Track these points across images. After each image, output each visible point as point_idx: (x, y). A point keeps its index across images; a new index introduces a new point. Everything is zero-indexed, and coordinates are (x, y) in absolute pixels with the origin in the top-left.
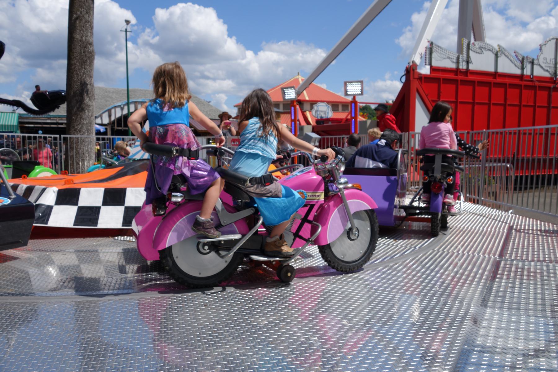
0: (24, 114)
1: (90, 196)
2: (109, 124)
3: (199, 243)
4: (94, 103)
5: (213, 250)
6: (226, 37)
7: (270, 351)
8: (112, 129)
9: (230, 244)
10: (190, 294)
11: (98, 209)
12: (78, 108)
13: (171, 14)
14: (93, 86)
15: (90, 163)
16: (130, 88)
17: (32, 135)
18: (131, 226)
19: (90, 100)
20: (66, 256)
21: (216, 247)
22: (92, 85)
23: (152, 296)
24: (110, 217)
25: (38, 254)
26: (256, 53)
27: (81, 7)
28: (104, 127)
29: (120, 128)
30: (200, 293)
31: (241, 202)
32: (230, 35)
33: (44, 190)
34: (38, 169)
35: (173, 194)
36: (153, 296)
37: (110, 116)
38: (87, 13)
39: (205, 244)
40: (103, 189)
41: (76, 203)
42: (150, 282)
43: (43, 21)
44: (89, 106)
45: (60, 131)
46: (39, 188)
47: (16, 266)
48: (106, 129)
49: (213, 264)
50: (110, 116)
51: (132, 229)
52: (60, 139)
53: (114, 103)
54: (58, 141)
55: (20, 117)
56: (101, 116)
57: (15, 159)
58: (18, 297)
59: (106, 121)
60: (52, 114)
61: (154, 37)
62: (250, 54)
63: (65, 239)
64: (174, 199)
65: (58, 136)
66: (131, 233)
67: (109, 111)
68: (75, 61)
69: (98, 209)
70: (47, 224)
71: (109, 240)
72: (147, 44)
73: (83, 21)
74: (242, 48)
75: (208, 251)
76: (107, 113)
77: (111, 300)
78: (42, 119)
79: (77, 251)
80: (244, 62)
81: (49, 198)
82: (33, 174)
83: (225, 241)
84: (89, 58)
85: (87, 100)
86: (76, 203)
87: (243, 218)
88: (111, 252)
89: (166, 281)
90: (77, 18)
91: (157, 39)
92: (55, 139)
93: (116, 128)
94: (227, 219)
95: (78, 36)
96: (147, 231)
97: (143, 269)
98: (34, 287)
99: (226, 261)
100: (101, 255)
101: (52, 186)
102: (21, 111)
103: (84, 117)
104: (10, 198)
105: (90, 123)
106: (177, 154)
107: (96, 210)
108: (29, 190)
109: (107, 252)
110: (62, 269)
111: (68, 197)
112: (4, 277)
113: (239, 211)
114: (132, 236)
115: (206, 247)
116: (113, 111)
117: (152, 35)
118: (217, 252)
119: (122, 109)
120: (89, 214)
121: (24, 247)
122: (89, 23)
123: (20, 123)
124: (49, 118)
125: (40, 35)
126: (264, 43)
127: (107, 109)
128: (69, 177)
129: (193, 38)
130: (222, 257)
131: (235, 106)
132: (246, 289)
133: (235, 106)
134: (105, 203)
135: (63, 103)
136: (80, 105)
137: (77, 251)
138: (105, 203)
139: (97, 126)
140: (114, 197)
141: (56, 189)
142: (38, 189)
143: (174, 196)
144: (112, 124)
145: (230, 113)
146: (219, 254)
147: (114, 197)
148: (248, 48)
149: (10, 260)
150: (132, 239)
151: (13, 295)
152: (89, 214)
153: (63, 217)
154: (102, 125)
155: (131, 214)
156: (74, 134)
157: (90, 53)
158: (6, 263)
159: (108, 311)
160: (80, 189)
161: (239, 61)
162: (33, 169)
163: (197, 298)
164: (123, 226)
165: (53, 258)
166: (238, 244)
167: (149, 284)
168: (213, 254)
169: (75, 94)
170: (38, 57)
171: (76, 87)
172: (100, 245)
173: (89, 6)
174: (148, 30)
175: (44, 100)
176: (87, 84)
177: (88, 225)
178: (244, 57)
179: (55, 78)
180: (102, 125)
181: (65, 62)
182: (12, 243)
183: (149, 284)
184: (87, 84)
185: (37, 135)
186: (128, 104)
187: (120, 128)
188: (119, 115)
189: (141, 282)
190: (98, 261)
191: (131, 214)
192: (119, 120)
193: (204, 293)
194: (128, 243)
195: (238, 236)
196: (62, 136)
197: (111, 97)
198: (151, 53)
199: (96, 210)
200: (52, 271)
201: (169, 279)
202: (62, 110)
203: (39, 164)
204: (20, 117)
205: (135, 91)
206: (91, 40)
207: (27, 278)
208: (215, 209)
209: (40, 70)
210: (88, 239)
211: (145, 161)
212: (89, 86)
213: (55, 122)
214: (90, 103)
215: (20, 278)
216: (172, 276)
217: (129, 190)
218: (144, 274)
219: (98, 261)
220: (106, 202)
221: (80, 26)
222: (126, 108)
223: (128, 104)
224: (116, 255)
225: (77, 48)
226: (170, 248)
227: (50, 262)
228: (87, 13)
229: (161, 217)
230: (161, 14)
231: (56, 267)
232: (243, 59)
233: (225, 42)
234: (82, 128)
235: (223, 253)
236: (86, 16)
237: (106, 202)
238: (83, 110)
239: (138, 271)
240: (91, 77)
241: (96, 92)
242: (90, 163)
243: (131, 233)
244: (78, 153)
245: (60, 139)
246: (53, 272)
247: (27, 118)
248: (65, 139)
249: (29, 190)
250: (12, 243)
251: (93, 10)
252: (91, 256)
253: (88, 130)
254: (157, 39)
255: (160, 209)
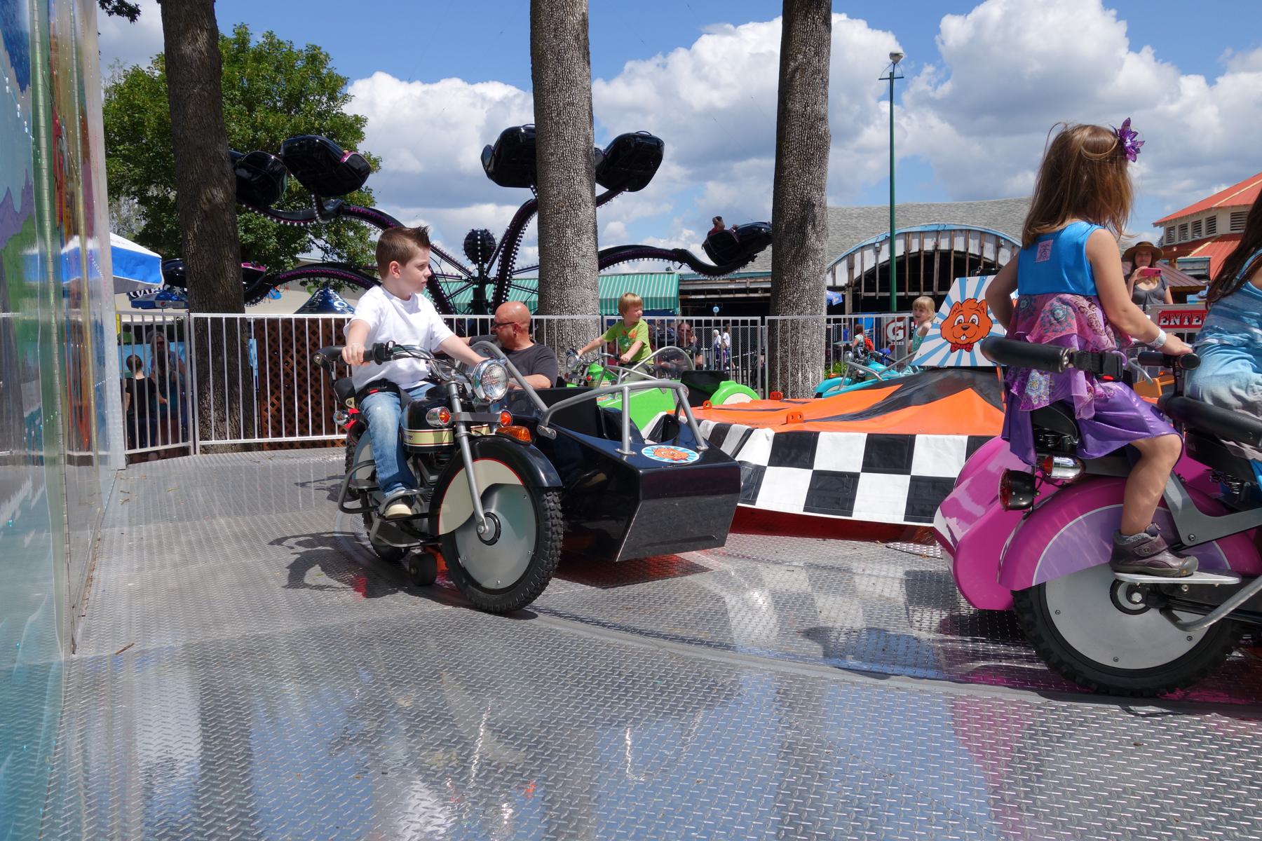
0: (689, 275)
1: (840, 450)
2: (848, 285)
3: (1116, 584)
4: (826, 245)
5: (1155, 606)
6: (1123, 51)
7: (1094, 816)
8: (856, 298)
9: (1204, 599)
10: (1089, 706)
11: (854, 477)
12: (794, 257)
13: (979, 25)
14: (825, 208)
15: (815, 375)
16: (896, 204)
17: (703, 318)
18: (931, 521)
19: (818, 239)
20: (795, 575)
21: (1164, 599)
22: (822, 206)
23: (971, 692)
24: (881, 499)
25: (741, 564)
26: (1211, 82)
27: (806, 43)
28: (839, 294)
29: (873, 294)
30: (1116, 708)
31: (1241, 487)
32: (1135, 47)
33: (748, 434)
34: (726, 387)
35: (1056, 460)
36: (999, 695)
37: (851, 269)
38: (816, 54)
39: (1132, 588)
40: (865, 436)
41: (809, 465)
42: (984, 659)
43: (715, 86)
44: (816, 251)
45: (762, 306)
46: (738, 429)
47: (706, 585)
48: (843, 296)
49: (1154, 641)
50: (851, 269)
51: (933, 528)
52: (763, 323)
53: (860, 240)
54: (759, 326)
55: (682, 280)
56: (832, 270)
57: (685, 368)
58: (719, 652)
59: (842, 280)
60: (742, 270)
61: (941, 82)
62: (1192, 85)
63: (788, 538)
64: (1057, 473)
65: (758, 318)
66: (932, 536)
67: (850, 257)
68: (789, 160)
69: (854, 477)
70: (753, 503)
71: (876, 548)
72: (924, 102)
73: (809, 73)
74: (1168, 70)
75: (1142, 606)
76: (845, 263)
77: (903, 689)
78: (720, 283)
79: (810, 566)
80: (1174, 108)
81: (757, 451)
82: (716, 399)
83: (1191, 586)
84: (819, 148)
85: (812, 240)
86: (809, 465)
87: (1244, 533)
88: (881, 575)
89: (1022, 663)
90: (796, 70)
91: (947, 88)
92: (754, 323)
93: (863, 294)
94: (1201, 527)
95: (797, 107)
96: (984, 537)
97: (954, 625)
98: (735, 635)
99: (1190, 638)
100: (857, 579)
101: (764, 426)
102: (686, 269)
103: (805, 275)
104: (697, 451)
105: (818, 288)
106: (1071, 366)
107: (849, 481)
108: (720, 433)
109: (877, 577)
110: (781, 602)
111: (796, 449)
112: (688, 605)
113: (1232, 510)
114: (933, 544)
115: (1137, 597)
116: (858, 256)
117: (935, 80)
118: (1166, 611)
119: (877, 251)
120: (835, 489)
121: (720, 549)
122: (821, 74)
123: (681, 292)
124: (732, 281)
125: (711, 113)
126: (1229, 52)
127: (845, 253)
128: (789, 407)
129: (1036, 67)
130: (1184, 627)
131: (1155, 225)
132: (1249, 720)
133: (1155, 225)
134: (869, 466)
135: (763, 248)
136: (798, 252)
137: (810, 566)
138: (869, 466)
139: (828, 293)
140: (889, 454)
141: (770, 433)
142: (736, 432)
143: (1058, 465)
144: (855, 285)
145: (624, 199)
146: (1174, 620)
147: (889, 454)
148: (1186, 70)
149: (694, 572)
150: (936, 550)
151: (709, 644)
152: (835, 489)
153: (784, 491)
154: (833, 289)
155: (928, 495)
156: (777, 314)
157: (821, 138)
158: (689, 577)
159: (901, 713)
160: (817, 434)
161: (1160, 107)
162: (717, 387)
163: (1108, 717)
164: (906, 520)
165: (764, 573)
166: (1230, 601)
167: (983, 663)
168: (1153, 615)
169: (792, 227)
170: (715, 157)
171: (793, 211)
172: (859, 558)
173: (821, 38)
174: (929, 69)
175: (730, 246)
176: (814, 205)
177: (829, 513)
178: (1176, 94)
179: (750, 198)
180: (833, 289)
181: (771, 162)
182: (699, 539)
183: (983, 663)
184: (814, 205)
185: (712, 318)
186: (891, 240)
187: (873, 294)
188: (869, 264)
189: (954, 657)
190: (849, 591)
191: (928, 495)
192: (870, 275)
193: (1129, 711)
194: (919, 559)
195: (1231, 580)
196: (767, 318)
197: (855, 228)
198: (933, 120)
199: (849, 481)
200: (759, 598)
201: (1030, 659)
202: (762, 262)
203: (726, 378)
204: (682, 280)
205: (906, 209)
206: (823, 111)
207: (720, 615)
208: (1163, 502)
209: (711, 185)
210: (833, 541)
211: (950, 373)
212: (817, 209)
213: (743, 286)
214: (818, 245)
215: (716, 612)
216: (1043, 655)
217: (919, 439)
218: (968, 639)
219: (849, 591)
220: (870, 465)
221: (801, 85)
222: (886, 248)
223: (891, 240)
224: (897, 585)
225: (796, 132)
226: (1041, 588)
227: (758, 582)
228: (816, 54)
229: (1022, 514)
230: (954, 28)
231: (766, 592)
232: (1172, 102)
233: (1120, 65)
234: (800, 298)
235: (1185, 617)
236: (815, 61)
237: (870, 465)
238: (804, 258)
239: (944, 627)
240: (821, 189)
241: (831, 221)
242: (815, 375)
243: (932, 536)
244: (794, 353)
245: (763, 323)
246: (760, 601)
247: (693, 282)
248: (772, 323)
249: (720, 433)
250: (699, 539)
251: (829, 45)
252: (836, 578)
253: (813, 303)
254: (947, 88)
255: (1020, 493)
